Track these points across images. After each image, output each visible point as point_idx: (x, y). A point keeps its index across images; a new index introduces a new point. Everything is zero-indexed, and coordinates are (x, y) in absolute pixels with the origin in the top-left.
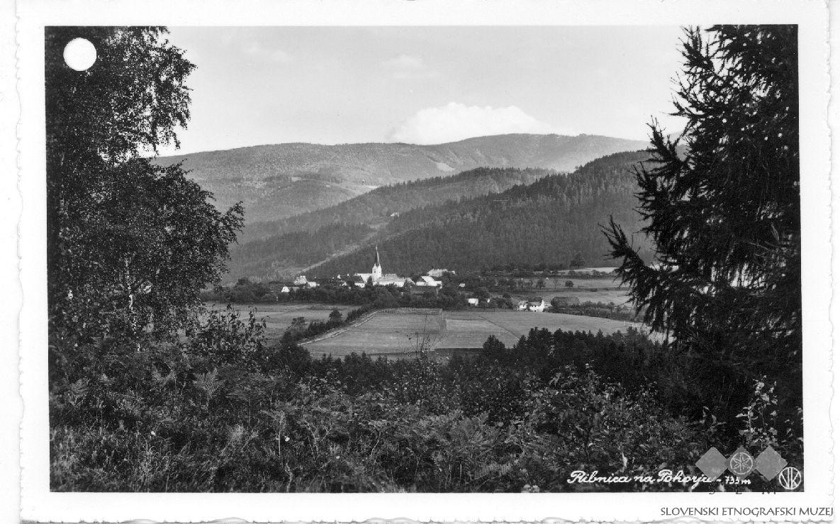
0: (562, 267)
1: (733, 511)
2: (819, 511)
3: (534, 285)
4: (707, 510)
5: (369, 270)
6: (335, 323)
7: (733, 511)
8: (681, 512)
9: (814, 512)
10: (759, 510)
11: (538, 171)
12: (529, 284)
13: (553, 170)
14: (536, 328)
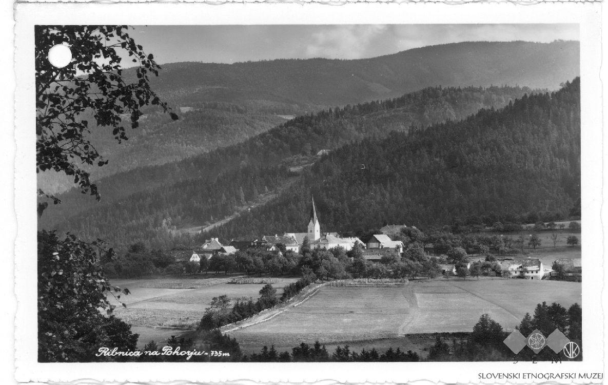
0: (559, 218)
1: (530, 375)
2: (593, 375)
3: (526, 242)
4: (512, 375)
5: (302, 228)
6: (268, 301)
7: (530, 375)
8: (493, 376)
9: (589, 376)
10: (549, 375)
11: (506, 90)
12: (518, 241)
13: (525, 88)
14: (544, 303)
